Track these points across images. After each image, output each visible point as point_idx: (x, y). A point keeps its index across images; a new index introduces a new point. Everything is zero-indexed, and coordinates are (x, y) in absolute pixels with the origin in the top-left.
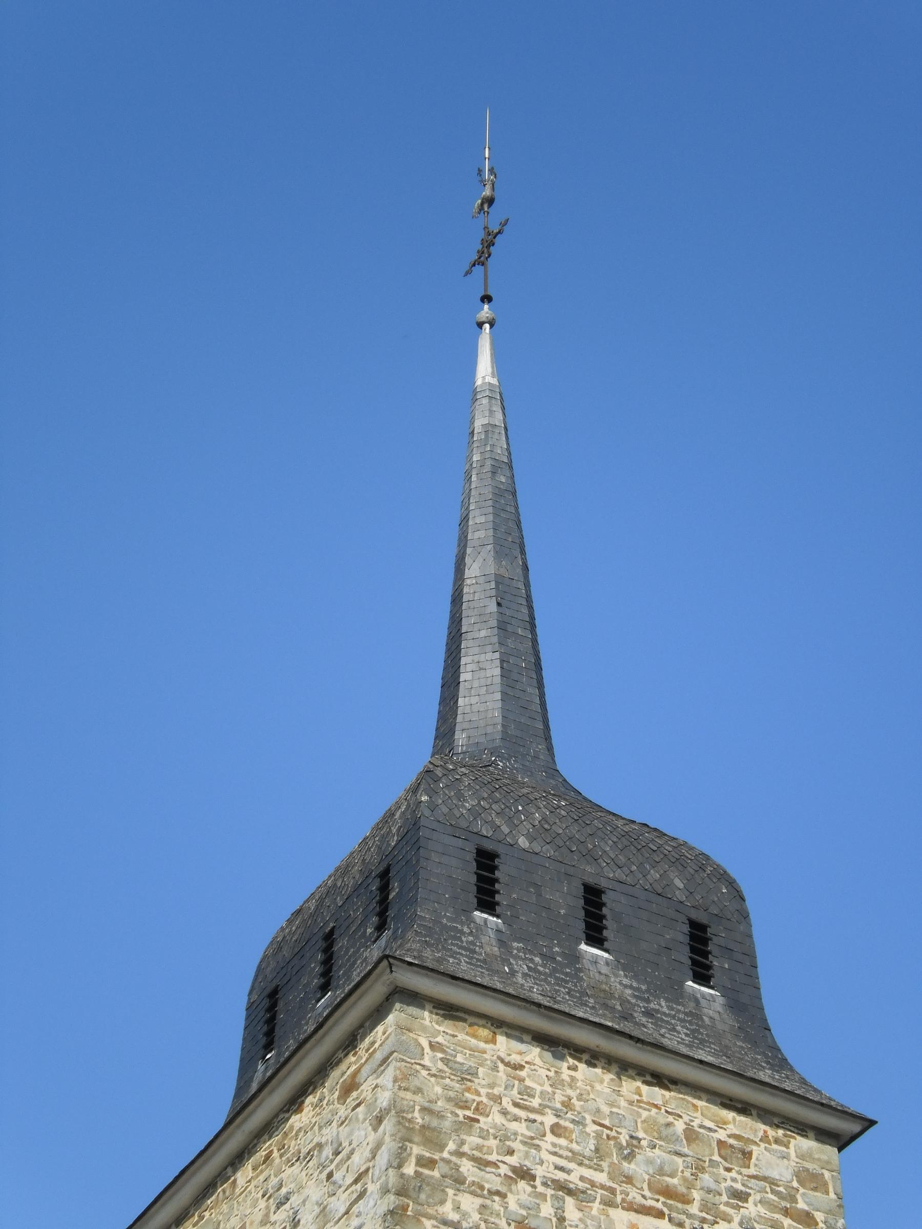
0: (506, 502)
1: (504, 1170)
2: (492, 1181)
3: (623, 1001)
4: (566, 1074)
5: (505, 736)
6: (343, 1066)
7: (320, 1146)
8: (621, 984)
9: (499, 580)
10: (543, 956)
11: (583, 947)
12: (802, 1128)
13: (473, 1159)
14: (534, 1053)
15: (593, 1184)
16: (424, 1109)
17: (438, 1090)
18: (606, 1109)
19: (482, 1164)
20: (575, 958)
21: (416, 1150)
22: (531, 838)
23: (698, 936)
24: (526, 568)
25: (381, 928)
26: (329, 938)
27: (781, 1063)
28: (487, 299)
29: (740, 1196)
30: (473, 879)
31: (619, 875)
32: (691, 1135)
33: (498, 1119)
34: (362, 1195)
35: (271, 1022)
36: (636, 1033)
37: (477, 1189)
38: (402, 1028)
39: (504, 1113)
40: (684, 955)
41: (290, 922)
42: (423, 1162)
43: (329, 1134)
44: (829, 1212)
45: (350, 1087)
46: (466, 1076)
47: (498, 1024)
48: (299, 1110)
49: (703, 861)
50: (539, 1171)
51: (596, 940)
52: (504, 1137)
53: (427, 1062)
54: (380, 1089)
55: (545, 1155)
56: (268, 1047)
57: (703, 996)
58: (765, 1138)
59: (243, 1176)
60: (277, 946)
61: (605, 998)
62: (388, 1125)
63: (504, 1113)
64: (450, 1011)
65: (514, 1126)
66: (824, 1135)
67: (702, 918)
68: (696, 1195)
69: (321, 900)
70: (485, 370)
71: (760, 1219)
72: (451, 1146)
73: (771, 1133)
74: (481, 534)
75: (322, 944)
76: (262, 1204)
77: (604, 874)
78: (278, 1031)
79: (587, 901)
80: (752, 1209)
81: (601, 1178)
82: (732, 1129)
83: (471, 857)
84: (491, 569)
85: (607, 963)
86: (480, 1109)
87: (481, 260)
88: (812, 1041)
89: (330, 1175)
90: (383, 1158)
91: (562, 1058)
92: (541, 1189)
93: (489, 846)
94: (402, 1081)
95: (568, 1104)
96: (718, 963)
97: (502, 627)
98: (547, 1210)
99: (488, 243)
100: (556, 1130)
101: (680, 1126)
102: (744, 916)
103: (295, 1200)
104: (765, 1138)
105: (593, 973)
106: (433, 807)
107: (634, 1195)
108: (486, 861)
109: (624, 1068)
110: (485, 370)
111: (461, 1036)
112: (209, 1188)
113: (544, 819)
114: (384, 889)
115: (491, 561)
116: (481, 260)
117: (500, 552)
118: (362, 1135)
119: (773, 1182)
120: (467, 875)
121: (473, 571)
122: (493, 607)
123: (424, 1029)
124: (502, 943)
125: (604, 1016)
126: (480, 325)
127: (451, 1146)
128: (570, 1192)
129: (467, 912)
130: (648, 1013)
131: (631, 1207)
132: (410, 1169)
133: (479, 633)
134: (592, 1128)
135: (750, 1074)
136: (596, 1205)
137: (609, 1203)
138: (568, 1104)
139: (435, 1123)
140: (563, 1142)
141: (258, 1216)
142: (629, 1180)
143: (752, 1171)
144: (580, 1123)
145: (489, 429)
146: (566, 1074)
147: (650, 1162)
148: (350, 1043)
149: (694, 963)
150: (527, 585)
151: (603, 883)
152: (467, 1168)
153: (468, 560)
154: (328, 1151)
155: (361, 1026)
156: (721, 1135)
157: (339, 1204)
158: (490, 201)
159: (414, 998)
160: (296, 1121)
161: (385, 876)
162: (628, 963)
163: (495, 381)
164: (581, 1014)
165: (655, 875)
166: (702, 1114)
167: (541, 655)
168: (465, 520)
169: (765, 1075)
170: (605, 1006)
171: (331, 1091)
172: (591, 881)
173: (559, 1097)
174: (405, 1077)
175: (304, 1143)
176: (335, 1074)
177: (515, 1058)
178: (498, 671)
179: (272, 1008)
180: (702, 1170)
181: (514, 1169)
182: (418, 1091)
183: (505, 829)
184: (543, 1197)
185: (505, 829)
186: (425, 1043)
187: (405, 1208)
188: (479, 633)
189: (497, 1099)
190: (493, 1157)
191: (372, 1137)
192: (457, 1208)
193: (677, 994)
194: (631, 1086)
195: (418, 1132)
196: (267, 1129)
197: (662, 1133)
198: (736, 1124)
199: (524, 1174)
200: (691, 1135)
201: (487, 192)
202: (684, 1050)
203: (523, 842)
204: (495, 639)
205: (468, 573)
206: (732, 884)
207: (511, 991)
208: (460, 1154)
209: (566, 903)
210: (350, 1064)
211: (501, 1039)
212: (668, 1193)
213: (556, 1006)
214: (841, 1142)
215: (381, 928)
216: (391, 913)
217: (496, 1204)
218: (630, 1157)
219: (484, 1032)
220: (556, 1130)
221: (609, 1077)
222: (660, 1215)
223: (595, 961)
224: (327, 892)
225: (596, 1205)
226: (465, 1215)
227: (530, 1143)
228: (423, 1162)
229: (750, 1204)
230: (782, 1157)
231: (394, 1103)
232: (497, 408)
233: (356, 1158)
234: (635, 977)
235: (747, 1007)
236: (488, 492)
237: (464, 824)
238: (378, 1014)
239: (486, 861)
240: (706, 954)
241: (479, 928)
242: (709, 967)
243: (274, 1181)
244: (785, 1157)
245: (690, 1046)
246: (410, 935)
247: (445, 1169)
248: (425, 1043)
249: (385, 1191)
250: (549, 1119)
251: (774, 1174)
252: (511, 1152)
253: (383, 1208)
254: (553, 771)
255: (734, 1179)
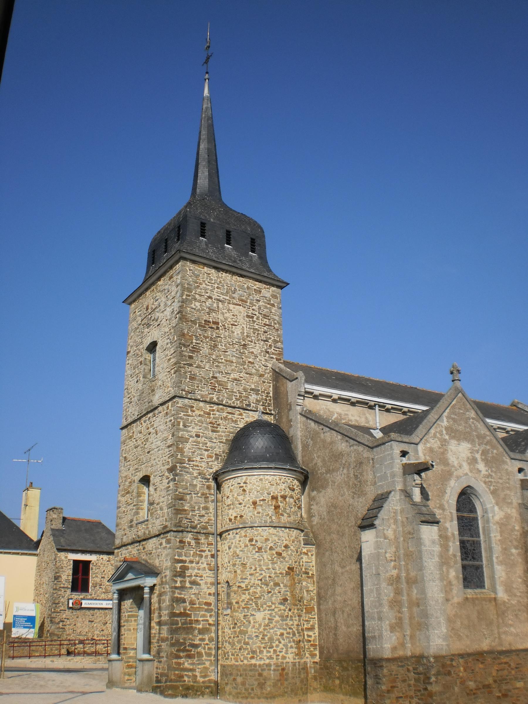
0: (211, 129)
1: (205, 297)
2: (203, 299)
3: (234, 258)
4: (220, 275)
5: (209, 190)
6: (169, 273)
7: (164, 289)
8: (234, 254)
9: (208, 149)
10: (216, 248)
11: (226, 245)
12: (273, 285)
13: (199, 294)
14: (213, 271)
15: (225, 299)
16: (187, 284)
17: (191, 279)
18: (229, 283)
19: (201, 295)
20: (223, 248)
21: (186, 293)
22: (214, 219)
23: (253, 241)
24: (215, 146)
25: (178, 240)
26: (166, 240)
27: (269, 271)
28: (207, 73)
29: (259, 301)
30: (200, 229)
31: (235, 227)
32: (248, 288)
33: (205, 286)
34: (174, 302)
35: (154, 257)
36: (236, 266)
37: (199, 301)
38: (182, 266)
39: (206, 284)
40: (249, 246)
41: (158, 234)
42: (187, 295)
43: (166, 287)
44: (278, 303)
45: (171, 277)
46: (197, 276)
47: (205, 265)
48: (160, 281)
49: (255, 223)
50: (213, 297)
51: (229, 244)
52: (206, 289)
53: (188, 273)
54: (178, 279)
55: (215, 293)
56: (153, 264)
57: (253, 255)
58: (265, 288)
59: (148, 293)
60: (155, 240)
61: (230, 257)
62: (179, 287)
63: (206, 284)
64: (194, 262)
65: (208, 287)
66: (278, 287)
67: (253, 237)
68: (249, 301)
69: (164, 230)
70: (206, 92)
71: (263, 305)
72: (194, 292)
73: (266, 287)
74: (204, 136)
75: (165, 241)
76: (152, 300)
77: (231, 227)
78: (155, 260)
79: (227, 234)
80: (261, 303)
81: (228, 298)
82: (257, 286)
83: (199, 224)
84: (206, 147)
85: (231, 249)
86: (200, 284)
87: (206, 62)
88: (277, 264)
89: (167, 296)
90: (178, 294)
91: (219, 272)
92: (214, 301)
93: (203, 221)
94: (183, 278)
95: (220, 282)
96: (257, 248)
97: (209, 162)
98: (215, 305)
99: (208, 58)
100: (218, 288)
101: (246, 286)
102: (264, 236)
103: (159, 300)
104: (265, 288)
105: (228, 251)
106: (190, 212)
107: (235, 301)
108: (203, 225)
109: (234, 274)
110: (206, 92)
111: (196, 267)
112: (140, 295)
113: (217, 214)
114: (179, 231)
115: (206, 144)
116: (206, 62)
117: (209, 142)
118: (174, 289)
119: (266, 297)
120: (198, 228)
121: (202, 146)
122: (207, 157)
123: (188, 266)
124: (206, 245)
125: (229, 262)
126: (205, 80)
127: (194, 292)
128: (220, 301)
129: (198, 238)
130: (240, 260)
131: (234, 304)
132: (184, 297)
133: (204, 132)
134: (226, 287)
135: (262, 274)
136: (226, 304)
137: (229, 303)
138: (220, 282)
139: (190, 287)
140: (219, 290)
141: (152, 303)
142: (234, 298)
143: (261, 295)
144: (223, 286)
145: (207, 108)
146: (220, 275)
147: (239, 294)
148: (171, 267)
149: (251, 248)
150: (215, 150)
151: (231, 230)
152: (197, 296)
153: (201, 143)
154: (166, 291)
155: (173, 264)
156: (255, 287)
157: (169, 303)
158: (209, 47)
159: (185, 259)
160: (159, 283)
161: (179, 227)
162: (235, 249)
163: (208, 95)
164: (224, 262)
165: (243, 227)
166: (250, 283)
167: (218, 157)
168: (200, 132)
169: (265, 274)
170: (230, 259)
171: (167, 277)
172: (228, 229)
173: (219, 280)
174: (183, 277)
175: (161, 288)
176: (168, 274)
177: (209, 272)
178: (207, 174)
179: (154, 254)
180: (250, 295)
181: (208, 297)
182: (186, 280)
183: (208, 217)
184: (214, 302)
185: (208, 217)
186: (188, 269)
187: (183, 305)
188: (204, 132)
189: (204, 281)
190: (203, 294)
191: (176, 289)
192: (195, 305)
193: (247, 255)
194: (235, 278)
195: (186, 289)
196: (153, 284)
197: (242, 287)
198: (258, 285)
199: (210, 297)
200: (248, 288)
201: (208, 44)
202: (247, 269)
203: (212, 220)
204: (207, 165)
205: (201, 147)
206: (261, 229)
207: (208, 257)
208: (196, 294)
209: (222, 234)
210: (171, 272)
211: (205, 268)
212: (242, 300)
213: (218, 261)
214: (281, 288)
215: (178, 240)
216: (180, 237)
217: (204, 304)
218: (234, 293)
219: (202, 266)
220: (218, 288)
221: (230, 275)
222: (240, 305)
223: (228, 248)
224: (165, 229)
225: (226, 304)
226: (197, 307)
227: (211, 291)
228: (187, 295)
229: (260, 302)
230: (268, 292)
231: (181, 282)
232: (209, 102)
233: (173, 293)
234: (237, 252)
235: (263, 258)
236: (206, 125)
237: (197, 216)
238: (177, 262)
239: (203, 225)
240: (254, 246)
241: (201, 241)
242: (255, 249)
243: (155, 295)
244: (269, 292)
245: (249, 268)
246: (185, 243)
247: (192, 297)
248: (188, 269)
249: (179, 302)
250: (216, 285)
251: (266, 296)
252: (207, 293)
253: (178, 306)
254: (221, 199)
255: (257, 297)
